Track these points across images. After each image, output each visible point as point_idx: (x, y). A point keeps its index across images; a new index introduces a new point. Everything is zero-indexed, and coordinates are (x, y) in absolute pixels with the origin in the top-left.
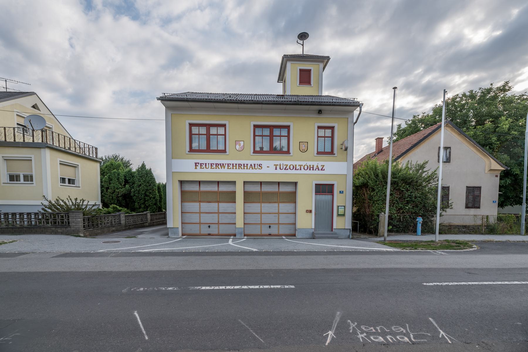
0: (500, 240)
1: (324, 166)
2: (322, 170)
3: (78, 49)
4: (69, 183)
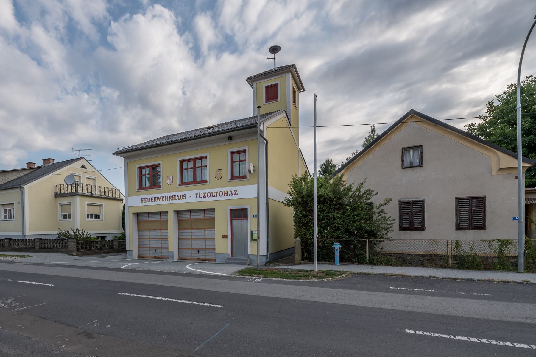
0: (417, 275)
1: (237, 191)
2: (235, 195)
3: (188, 94)
4: (96, 218)
